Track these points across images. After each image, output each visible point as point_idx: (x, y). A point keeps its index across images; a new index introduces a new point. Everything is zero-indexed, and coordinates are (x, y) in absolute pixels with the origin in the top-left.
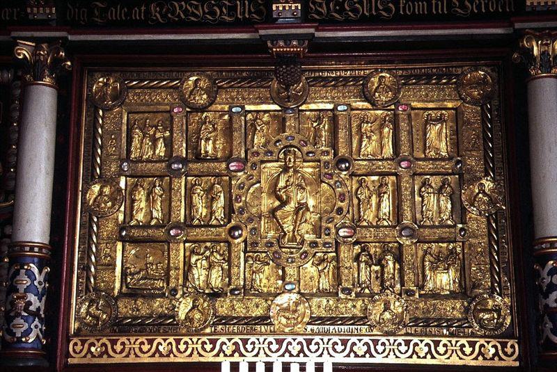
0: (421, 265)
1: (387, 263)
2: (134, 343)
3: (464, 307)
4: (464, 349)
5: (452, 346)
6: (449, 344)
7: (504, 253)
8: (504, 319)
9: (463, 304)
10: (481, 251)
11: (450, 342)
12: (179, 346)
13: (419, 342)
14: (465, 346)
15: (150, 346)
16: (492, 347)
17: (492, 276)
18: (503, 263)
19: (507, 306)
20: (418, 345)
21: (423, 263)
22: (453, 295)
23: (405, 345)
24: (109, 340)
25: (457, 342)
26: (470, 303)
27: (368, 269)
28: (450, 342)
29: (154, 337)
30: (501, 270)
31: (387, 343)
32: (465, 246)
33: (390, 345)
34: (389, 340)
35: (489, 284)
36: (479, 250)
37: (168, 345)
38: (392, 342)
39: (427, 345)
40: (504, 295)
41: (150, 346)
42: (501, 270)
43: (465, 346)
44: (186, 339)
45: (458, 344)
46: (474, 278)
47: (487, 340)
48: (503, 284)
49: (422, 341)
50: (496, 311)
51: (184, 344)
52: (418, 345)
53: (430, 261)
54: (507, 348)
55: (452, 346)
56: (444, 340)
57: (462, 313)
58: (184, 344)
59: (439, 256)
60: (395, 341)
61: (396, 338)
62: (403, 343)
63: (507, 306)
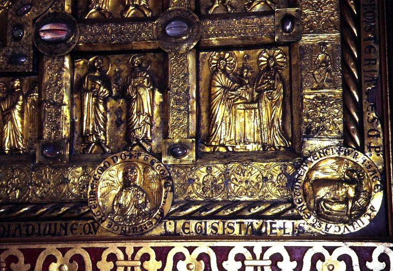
0: (206, 94)
1: (137, 93)
2: (261, 258)
3: (287, 175)
4: (279, 264)
5: (254, 257)
6: (248, 255)
7: (372, 62)
8: (369, 199)
9: (284, 172)
10: (324, 61)
11: (250, 249)
12: (224, 264)
13: (186, 252)
14: (281, 259)
15: (29, 265)
16: (340, 258)
17: (346, 112)
18: (369, 82)
19: (375, 172)
20: (184, 258)
21: (210, 89)
22: (266, 153)
23: (158, 259)
24: (214, 248)
25: (265, 249)
26: (297, 167)
27: (101, 107)
28: (250, 249)
29: (36, 246)
30: (365, 97)
31: (121, 256)
32: (293, 53)
33: (126, 258)
34: (123, 249)
35: (341, 127)
36: (321, 57)
37: (71, 261)
38: (258, 251)
39: (345, 258)
40: (370, 148)
41: (29, 265)
42: (365, 97)
43: (281, 259)
44: (113, 248)
45: (139, 254)
46: (308, 117)
47: (60, 246)
48: (367, 126)
49: (191, 249)
50: (351, 182)
51: (108, 260)
52: (184, 258)
53: (223, 87)
54: (371, 260)
55: (254, 257)
56: (239, 247)
57: (280, 188)
58: (108, 260)
59: (242, 75)
60: (136, 250)
61: (138, 245)
62: (153, 254)
63: (375, 172)
